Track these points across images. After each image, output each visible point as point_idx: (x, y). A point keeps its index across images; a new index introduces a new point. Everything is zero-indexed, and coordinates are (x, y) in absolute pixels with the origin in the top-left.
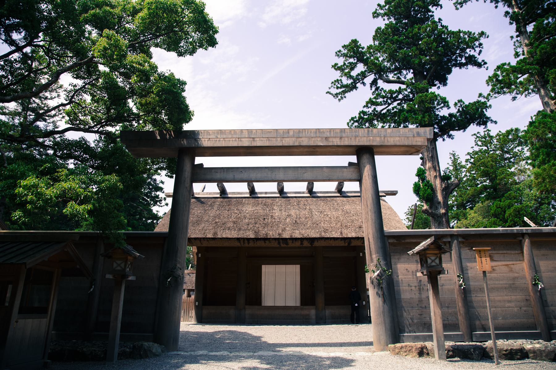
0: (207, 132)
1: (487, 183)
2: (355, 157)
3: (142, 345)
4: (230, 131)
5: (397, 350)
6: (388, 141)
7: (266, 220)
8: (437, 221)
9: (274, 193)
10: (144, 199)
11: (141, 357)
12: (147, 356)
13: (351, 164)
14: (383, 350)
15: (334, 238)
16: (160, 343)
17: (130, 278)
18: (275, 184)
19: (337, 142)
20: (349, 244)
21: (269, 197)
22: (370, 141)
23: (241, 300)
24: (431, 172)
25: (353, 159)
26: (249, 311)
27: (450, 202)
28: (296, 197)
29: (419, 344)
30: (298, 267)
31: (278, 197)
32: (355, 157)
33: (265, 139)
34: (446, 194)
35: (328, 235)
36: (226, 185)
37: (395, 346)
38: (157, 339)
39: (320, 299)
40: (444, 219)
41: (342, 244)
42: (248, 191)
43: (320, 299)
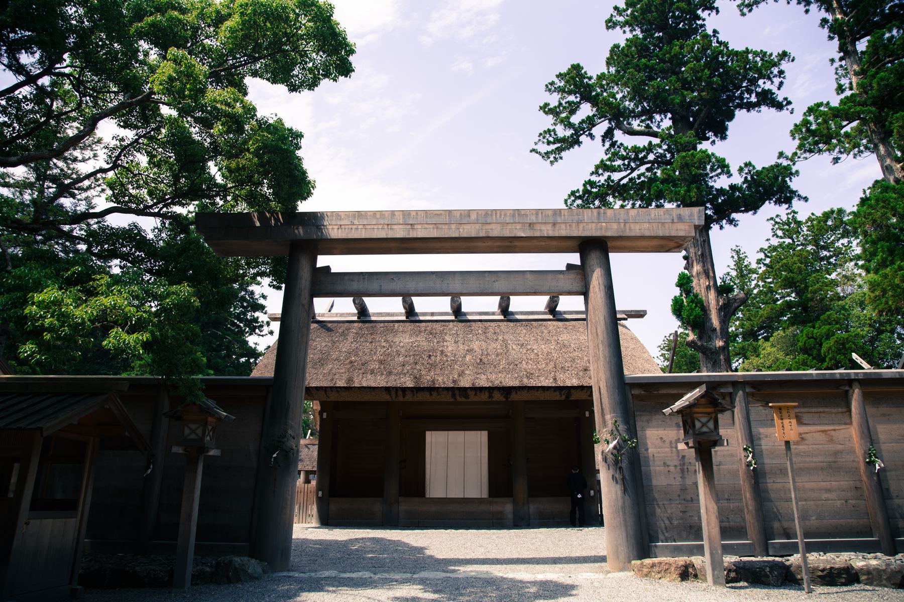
0: (337, 215)
1: (793, 297)
2: (578, 255)
3: (231, 561)
4: (375, 213)
5: (645, 570)
6: (630, 229)
7: (432, 358)
8: (711, 359)
9: (446, 314)
10: (234, 324)
11: (229, 581)
12: (239, 580)
13: (570, 267)
14: (622, 569)
15: (543, 388)
16: (260, 558)
17: (212, 453)
18: (448, 299)
19: (547, 231)
20: (568, 396)
21: (437, 321)
22: (601, 229)
23: (392, 487)
24: (702, 281)
25: (575, 258)
26: (405, 506)
27: (732, 329)
28: (481, 321)
29: (682, 560)
30: (484, 435)
31: (452, 321)
32: (578, 255)
33: (431, 226)
34: (725, 316)
35: (533, 383)
36: (367, 301)
37: (642, 563)
38: (256, 552)
39: (521, 486)
40: (722, 357)
41: (556, 397)
42: (403, 311)
43: (521, 486)
